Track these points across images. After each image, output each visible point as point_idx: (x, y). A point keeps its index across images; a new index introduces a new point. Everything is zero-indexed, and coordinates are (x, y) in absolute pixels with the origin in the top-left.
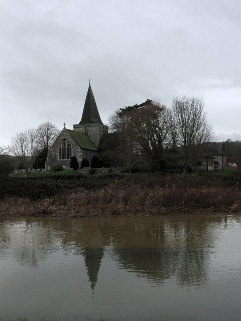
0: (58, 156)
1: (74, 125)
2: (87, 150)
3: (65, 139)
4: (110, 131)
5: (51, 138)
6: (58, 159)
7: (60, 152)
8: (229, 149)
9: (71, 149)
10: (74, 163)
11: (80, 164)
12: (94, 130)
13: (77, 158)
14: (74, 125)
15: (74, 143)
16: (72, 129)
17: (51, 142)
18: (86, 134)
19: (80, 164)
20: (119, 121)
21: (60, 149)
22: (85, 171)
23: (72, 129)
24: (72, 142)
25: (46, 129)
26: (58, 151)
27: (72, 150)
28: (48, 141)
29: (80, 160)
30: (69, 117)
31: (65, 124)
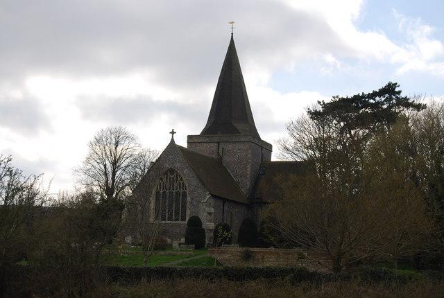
0: (152, 212)
1: (189, 137)
2: (224, 200)
3: (172, 171)
4: (275, 157)
5: (123, 165)
6: (151, 220)
7: (157, 199)
8: (431, 127)
9: (185, 195)
10: (195, 234)
11: (209, 235)
12: (235, 154)
13: (202, 218)
14: (189, 137)
15: (195, 182)
16: (185, 145)
17: (123, 176)
18: (219, 161)
19: (209, 235)
20: (311, 124)
21: (158, 193)
22: (230, 255)
23: (185, 145)
24: (189, 178)
25: (114, 141)
26: (153, 200)
27: (189, 199)
28: (114, 173)
29: (209, 225)
30: (168, 118)
31: (173, 133)
